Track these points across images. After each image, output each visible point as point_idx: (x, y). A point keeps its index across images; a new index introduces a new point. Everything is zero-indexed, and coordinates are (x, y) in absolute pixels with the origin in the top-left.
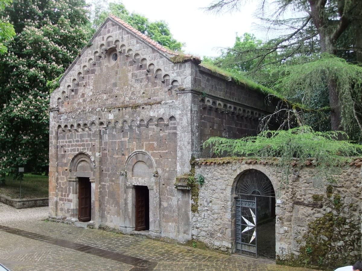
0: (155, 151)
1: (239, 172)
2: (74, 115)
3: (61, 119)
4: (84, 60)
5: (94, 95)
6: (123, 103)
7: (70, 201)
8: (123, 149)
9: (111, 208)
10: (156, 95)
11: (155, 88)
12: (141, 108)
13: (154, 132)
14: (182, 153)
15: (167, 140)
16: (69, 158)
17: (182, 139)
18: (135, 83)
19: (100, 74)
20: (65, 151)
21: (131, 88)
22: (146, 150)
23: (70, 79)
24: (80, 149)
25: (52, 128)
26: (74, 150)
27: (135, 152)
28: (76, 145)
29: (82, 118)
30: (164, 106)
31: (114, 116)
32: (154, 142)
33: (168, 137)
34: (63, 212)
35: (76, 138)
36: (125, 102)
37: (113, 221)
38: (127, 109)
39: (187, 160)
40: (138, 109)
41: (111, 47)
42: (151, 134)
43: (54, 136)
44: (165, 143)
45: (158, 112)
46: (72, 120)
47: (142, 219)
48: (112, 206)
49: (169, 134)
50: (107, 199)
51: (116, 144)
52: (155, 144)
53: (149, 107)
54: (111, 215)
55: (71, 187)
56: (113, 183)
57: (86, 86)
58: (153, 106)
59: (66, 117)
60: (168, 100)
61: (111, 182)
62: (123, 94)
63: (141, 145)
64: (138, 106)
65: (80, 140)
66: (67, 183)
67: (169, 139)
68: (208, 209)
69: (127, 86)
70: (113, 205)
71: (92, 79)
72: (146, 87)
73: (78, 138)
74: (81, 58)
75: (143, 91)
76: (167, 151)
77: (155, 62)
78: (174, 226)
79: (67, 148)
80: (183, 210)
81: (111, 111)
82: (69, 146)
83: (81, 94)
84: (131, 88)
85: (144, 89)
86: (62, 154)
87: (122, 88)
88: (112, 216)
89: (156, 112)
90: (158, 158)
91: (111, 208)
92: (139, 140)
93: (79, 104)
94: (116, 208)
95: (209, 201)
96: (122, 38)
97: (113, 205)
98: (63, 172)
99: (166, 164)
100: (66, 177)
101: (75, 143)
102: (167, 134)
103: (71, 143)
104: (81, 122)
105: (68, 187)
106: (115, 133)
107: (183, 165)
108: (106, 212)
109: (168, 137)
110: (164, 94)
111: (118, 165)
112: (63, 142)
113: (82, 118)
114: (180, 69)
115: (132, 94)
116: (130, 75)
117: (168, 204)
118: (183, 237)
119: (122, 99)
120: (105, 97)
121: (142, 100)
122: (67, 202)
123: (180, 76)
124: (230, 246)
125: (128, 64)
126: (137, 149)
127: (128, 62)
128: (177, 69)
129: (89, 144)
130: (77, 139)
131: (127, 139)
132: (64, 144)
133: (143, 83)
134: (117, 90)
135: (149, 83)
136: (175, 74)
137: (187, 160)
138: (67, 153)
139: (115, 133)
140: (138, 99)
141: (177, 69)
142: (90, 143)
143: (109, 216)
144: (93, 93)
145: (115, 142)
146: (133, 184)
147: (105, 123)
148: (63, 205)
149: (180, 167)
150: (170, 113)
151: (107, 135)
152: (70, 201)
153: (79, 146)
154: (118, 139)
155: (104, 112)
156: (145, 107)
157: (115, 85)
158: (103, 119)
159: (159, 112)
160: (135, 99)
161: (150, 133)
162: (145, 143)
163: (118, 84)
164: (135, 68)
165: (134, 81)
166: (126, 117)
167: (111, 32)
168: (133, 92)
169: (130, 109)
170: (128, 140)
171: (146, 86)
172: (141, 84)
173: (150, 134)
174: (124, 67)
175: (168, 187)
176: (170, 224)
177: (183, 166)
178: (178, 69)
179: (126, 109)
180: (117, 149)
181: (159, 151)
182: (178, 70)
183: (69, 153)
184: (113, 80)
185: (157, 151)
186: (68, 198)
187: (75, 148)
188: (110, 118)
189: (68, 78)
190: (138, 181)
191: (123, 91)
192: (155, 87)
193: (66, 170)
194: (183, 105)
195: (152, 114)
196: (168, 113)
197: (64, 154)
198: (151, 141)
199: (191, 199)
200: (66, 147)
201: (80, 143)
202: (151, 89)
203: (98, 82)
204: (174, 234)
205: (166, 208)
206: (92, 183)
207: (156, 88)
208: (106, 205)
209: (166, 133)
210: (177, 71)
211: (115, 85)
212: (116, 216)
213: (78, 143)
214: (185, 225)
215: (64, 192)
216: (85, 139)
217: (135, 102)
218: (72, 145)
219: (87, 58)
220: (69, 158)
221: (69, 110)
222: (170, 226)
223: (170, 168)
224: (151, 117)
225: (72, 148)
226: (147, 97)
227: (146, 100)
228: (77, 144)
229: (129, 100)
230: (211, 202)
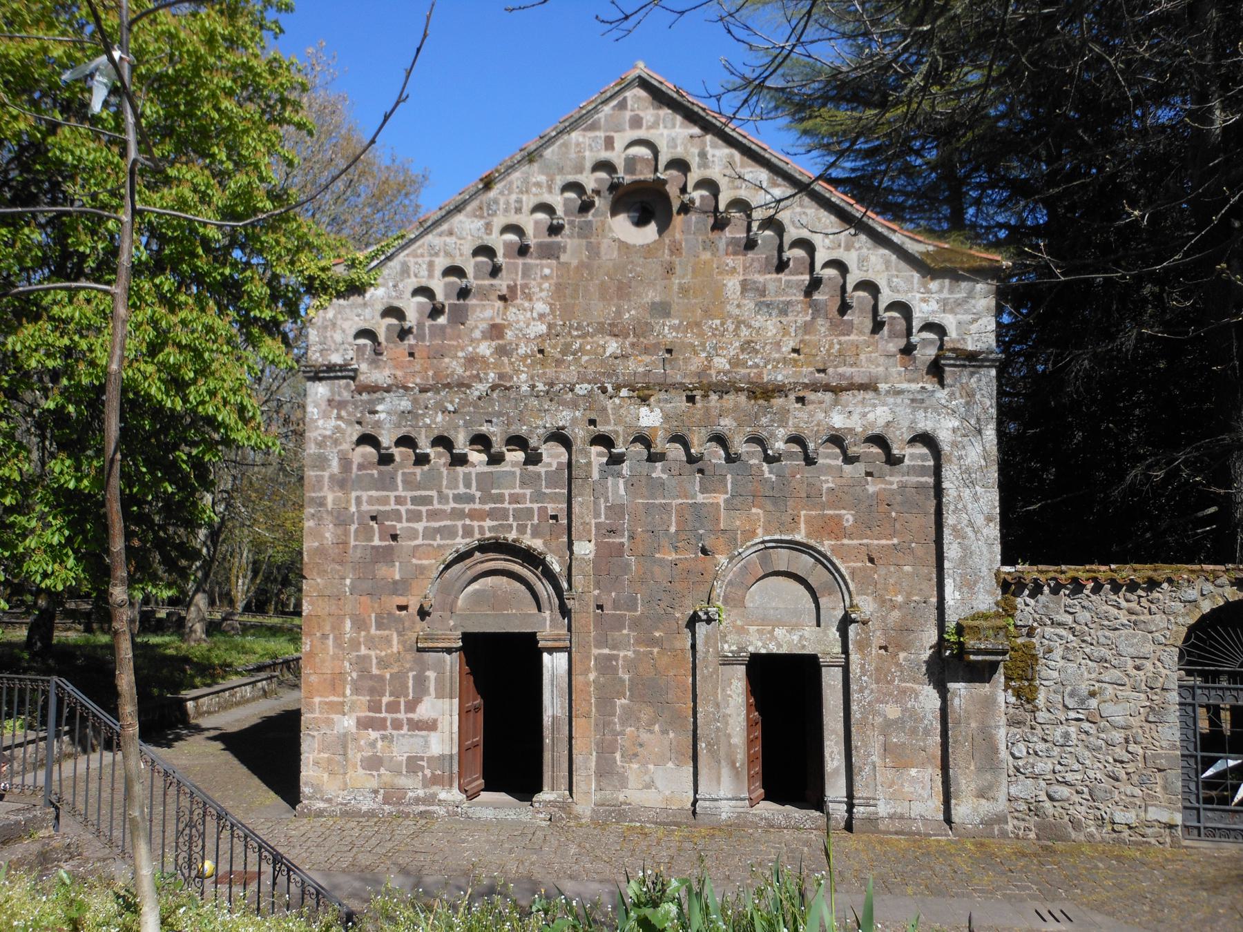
0: (846, 541)
1: (1206, 607)
2: (452, 402)
3: (375, 412)
4: (507, 203)
5: (552, 333)
6: (699, 375)
7: (431, 726)
8: (701, 532)
9: (644, 736)
10: (850, 360)
11: (843, 339)
12: (792, 397)
13: (844, 481)
14: (965, 548)
15: (896, 506)
16: (414, 561)
17: (965, 507)
18: (757, 313)
19: (582, 265)
20: (394, 537)
21: (738, 327)
22: (808, 535)
23: (431, 265)
24: (481, 528)
25: (320, 445)
26: (450, 533)
27: (763, 542)
28: (457, 514)
29: (500, 414)
30: (891, 400)
31: (667, 418)
32: (843, 512)
33: (899, 498)
34: (382, 771)
35: (456, 487)
36: (713, 372)
37: (658, 783)
38: (725, 397)
39: (984, 569)
40: (778, 402)
41: (642, 177)
42: (831, 485)
43: (332, 477)
44: (889, 517)
45: (864, 415)
46: (439, 418)
47: (510, 750)
48: (651, 732)
49: (903, 486)
50: (622, 706)
51: (669, 513)
52: (848, 518)
53: (829, 396)
54: (644, 765)
55: (431, 675)
56: (656, 650)
57: (514, 297)
58: (846, 397)
59: (405, 404)
60: (900, 382)
61: (648, 646)
62: (703, 344)
63: (786, 518)
64: (780, 390)
65: (478, 494)
66: (410, 656)
67: (902, 504)
68: (1081, 716)
69: (718, 322)
70: (657, 727)
71: (545, 277)
72: (806, 332)
73: (468, 485)
74: (492, 194)
75: (792, 344)
76: (895, 541)
77: (851, 259)
78: (927, 778)
79: (405, 524)
80: (973, 725)
81: (652, 399)
82: (415, 517)
83: (483, 326)
84: (738, 327)
85: (799, 338)
86: (373, 547)
87: (698, 324)
88: (651, 767)
89: (855, 417)
90: (860, 564)
91: (644, 736)
92: (775, 504)
93: (471, 361)
94: (672, 735)
95: (1086, 693)
96: (703, 155)
97: (657, 727)
98: (379, 617)
99: (892, 581)
100: (400, 634)
101: (452, 505)
102: (895, 486)
103: (431, 503)
104: (496, 432)
105: (411, 675)
106: (665, 476)
107: (968, 585)
108: (618, 756)
109: (899, 498)
110: (882, 360)
111: (678, 586)
112: (380, 501)
113: (500, 414)
114: (951, 291)
115: (743, 350)
116: (732, 284)
117: (904, 710)
118: (975, 810)
119: (696, 363)
120: (613, 346)
121: (790, 371)
122: (405, 731)
123: (952, 311)
124: (1178, 819)
125: (722, 245)
126: (766, 532)
127: (724, 240)
128: (941, 291)
129: (530, 510)
130: (462, 490)
131: (721, 499)
132: (387, 508)
133: (791, 318)
134: (670, 327)
135: (820, 321)
136: (934, 306)
137: (984, 569)
138: (403, 543)
139: (665, 476)
140: (770, 367)
141: (941, 291)
142: (535, 506)
143: (635, 766)
144: (550, 326)
145: (664, 506)
146: (751, 649)
147: (621, 439)
148: (380, 744)
149: (957, 593)
150: (913, 422)
151: (621, 481)
152: (431, 726)
153: (473, 515)
154: (678, 497)
155: (617, 401)
156: (811, 396)
157: (662, 309)
158: (607, 422)
159: (871, 417)
160: (757, 366)
161: (827, 481)
162: (803, 513)
163: (675, 307)
164: (755, 264)
165: (752, 305)
166: (722, 423)
167: (649, 128)
168: (748, 342)
169: (742, 398)
170: (726, 501)
171: (807, 328)
172: (783, 320)
173: (825, 486)
174: (706, 256)
175: (902, 655)
176: (913, 772)
177: (970, 588)
178: (945, 291)
179: (721, 397)
180: (673, 529)
181: (865, 541)
182: (945, 294)
183: (419, 541)
184: (651, 294)
185: (855, 542)
186: (410, 715)
187: (448, 523)
188: (644, 422)
189: (420, 260)
190: (773, 638)
191: (701, 335)
192: (844, 335)
193: (402, 608)
194: (967, 403)
195: (838, 421)
196: (905, 424)
197: (389, 549)
198: (830, 509)
199: (1005, 690)
200: (400, 521)
201: (477, 506)
202: (824, 338)
203: (576, 290)
204: (929, 803)
205: (895, 721)
206: (545, 655)
207: (847, 338)
208: (618, 728)
209: (892, 483)
210: (943, 296)
211: (662, 309)
212: (670, 765)
213: (467, 507)
214: (980, 770)
215: (386, 701)
216: (507, 492)
217: (760, 375)
218: (433, 515)
219: (524, 198)
220: (414, 561)
221: (418, 380)
222: (913, 781)
223: (909, 595)
224: (837, 430)
225: (436, 525)
226: (809, 364)
227: (806, 373)
228: (462, 510)
229: (728, 367)
230: (1092, 694)
